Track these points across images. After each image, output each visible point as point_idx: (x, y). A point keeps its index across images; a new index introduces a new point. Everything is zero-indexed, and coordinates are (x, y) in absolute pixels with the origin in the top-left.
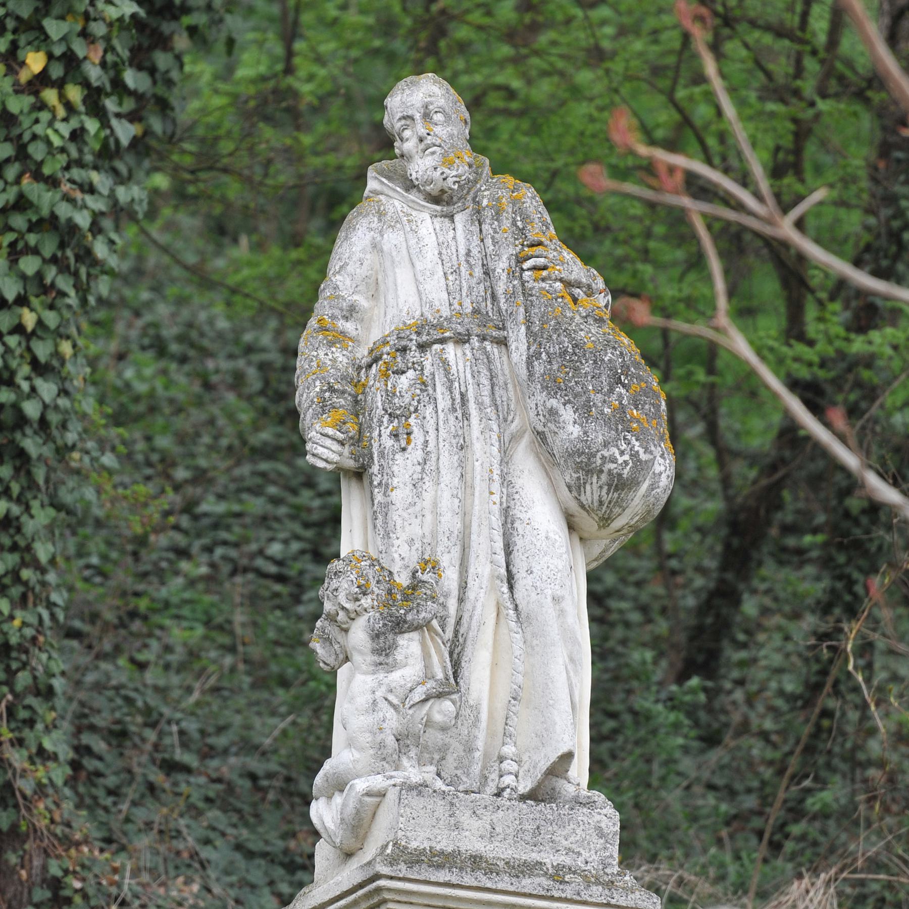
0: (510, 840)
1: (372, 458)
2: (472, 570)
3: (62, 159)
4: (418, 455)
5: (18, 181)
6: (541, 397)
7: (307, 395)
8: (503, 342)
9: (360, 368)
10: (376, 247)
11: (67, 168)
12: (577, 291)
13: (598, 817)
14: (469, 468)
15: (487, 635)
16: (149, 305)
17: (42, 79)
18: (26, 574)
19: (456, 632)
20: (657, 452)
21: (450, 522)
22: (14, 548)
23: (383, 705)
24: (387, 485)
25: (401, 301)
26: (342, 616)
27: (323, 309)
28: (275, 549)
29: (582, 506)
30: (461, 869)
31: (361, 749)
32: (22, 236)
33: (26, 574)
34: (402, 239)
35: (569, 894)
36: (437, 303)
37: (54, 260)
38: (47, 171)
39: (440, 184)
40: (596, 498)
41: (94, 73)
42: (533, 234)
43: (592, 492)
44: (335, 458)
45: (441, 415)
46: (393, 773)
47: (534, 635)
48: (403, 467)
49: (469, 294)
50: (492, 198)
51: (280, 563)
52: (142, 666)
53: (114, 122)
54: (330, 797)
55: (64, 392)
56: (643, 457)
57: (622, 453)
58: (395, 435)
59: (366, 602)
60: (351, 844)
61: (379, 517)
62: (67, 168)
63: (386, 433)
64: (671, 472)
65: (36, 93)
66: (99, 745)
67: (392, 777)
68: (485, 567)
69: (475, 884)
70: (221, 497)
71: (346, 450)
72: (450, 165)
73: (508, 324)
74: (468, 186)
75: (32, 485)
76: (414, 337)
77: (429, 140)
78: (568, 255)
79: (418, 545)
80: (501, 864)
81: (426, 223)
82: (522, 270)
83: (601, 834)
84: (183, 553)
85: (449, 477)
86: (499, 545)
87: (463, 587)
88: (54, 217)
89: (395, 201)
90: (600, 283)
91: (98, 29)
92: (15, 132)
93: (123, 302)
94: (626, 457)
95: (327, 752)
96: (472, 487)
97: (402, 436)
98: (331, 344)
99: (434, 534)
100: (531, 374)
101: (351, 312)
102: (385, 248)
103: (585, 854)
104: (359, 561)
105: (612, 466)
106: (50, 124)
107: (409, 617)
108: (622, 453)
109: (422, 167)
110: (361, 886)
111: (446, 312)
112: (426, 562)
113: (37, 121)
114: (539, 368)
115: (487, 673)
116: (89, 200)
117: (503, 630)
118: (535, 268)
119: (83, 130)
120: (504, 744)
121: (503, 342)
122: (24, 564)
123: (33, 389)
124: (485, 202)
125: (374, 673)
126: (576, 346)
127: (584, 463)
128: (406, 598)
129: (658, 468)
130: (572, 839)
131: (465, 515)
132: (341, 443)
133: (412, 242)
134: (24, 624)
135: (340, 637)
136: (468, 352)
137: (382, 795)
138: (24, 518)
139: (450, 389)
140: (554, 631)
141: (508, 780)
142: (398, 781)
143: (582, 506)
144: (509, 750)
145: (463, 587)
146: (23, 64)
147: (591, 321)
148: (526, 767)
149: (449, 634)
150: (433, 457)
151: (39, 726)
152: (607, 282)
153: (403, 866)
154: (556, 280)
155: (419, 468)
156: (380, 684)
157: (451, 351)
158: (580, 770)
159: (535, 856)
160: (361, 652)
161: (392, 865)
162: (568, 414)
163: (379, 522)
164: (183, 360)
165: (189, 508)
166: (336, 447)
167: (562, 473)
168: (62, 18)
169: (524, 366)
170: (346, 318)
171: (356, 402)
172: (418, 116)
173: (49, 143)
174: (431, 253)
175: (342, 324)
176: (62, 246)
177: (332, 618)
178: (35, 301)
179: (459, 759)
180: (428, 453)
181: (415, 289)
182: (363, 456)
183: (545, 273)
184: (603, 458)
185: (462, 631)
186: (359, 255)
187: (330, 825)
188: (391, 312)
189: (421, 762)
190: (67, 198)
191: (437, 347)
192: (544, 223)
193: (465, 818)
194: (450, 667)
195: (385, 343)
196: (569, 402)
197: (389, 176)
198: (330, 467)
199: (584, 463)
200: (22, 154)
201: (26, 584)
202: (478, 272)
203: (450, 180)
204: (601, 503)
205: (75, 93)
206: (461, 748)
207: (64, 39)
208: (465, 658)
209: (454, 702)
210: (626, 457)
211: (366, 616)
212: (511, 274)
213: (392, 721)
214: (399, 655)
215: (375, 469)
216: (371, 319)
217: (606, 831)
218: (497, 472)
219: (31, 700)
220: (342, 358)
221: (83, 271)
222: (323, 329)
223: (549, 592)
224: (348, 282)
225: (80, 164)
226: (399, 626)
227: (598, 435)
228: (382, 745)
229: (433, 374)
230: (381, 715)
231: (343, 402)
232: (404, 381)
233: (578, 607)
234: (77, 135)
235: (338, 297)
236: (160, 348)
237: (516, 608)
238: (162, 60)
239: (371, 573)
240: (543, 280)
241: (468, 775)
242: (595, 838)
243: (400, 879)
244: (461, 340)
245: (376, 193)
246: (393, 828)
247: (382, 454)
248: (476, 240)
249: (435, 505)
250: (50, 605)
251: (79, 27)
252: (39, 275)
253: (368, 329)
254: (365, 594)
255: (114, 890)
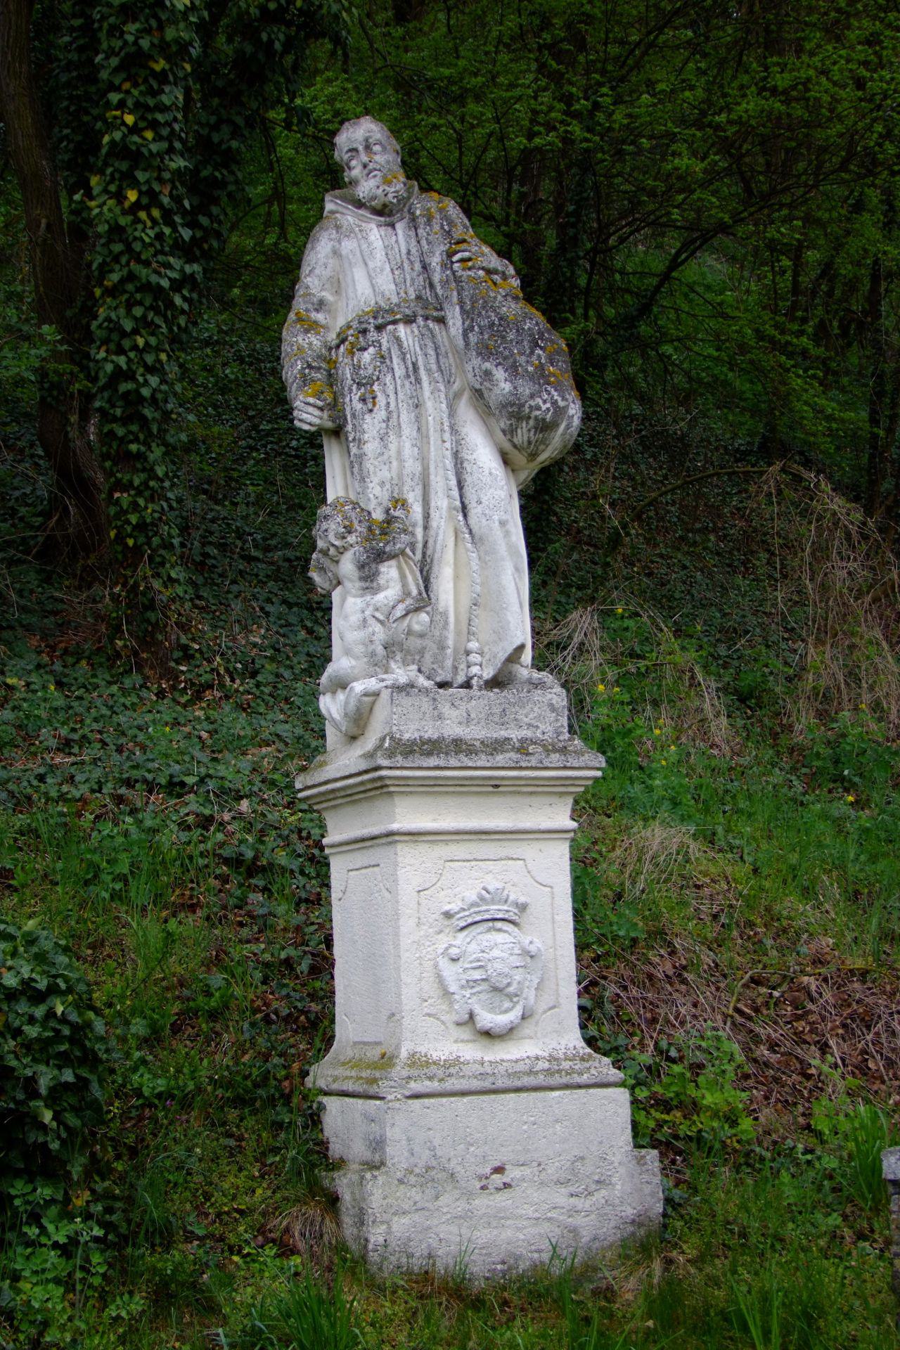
0: (483, 723)
1: (346, 419)
2: (433, 504)
3: (152, 250)
4: (383, 414)
5: (128, 264)
6: (476, 361)
7: (292, 370)
8: (441, 321)
9: (330, 349)
10: (336, 253)
11: (155, 255)
12: (495, 277)
13: (550, 696)
14: (423, 422)
15: (449, 556)
16: (236, 343)
17: (137, 206)
18: (152, 483)
19: (424, 554)
20: (570, 399)
21: (412, 466)
22: (144, 470)
23: (371, 621)
24: (360, 440)
25: (359, 293)
26: (332, 551)
27: (299, 304)
28: (294, 443)
29: (515, 446)
30: (447, 754)
31: (357, 658)
32: (132, 294)
33: (152, 483)
34: (355, 245)
35: (533, 764)
36: (387, 293)
37: (151, 308)
38: (143, 257)
39: (383, 199)
40: (526, 439)
41: (166, 200)
42: (458, 233)
43: (522, 435)
44: (317, 421)
45: (399, 382)
46: (385, 676)
47: (487, 553)
48: (372, 425)
49: (413, 284)
50: (423, 209)
51: (296, 450)
52: (236, 504)
53: (180, 229)
54: (334, 693)
55: (163, 381)
56: (561, 404)
57: (545, 402)
58: (363, 400)
59: (351, 539)
60: (355, 731)
61: (355, 465)
62: (155, 255)
63: (356, 398)
64: (579, 414)
65: (135, 214)
66: (214, 551)
67: (383, 680)
68: (442, 502)
69: (459, 765)
70: (268, 422)
71: (325, 415)
72: (389, 183)
73: (445, 306)
74: (403, 201)
75: (150, 434)
76: (372, 321)
77: (371, 166)
78: (486, 250)
79: (388, 486)
80: (477, 744)
81: (375, 233)
82: (452, 263)
83: (553, 708)
84: (252, 448)
85: (408, 430)
86: (454, 482)
87: (427, 516)
88: (149, 283)
89: (349, 217)
90: (511, 270)
91: (167, 175)
92: (124, 237)
93: (225, 343)
94: (548, 405)
95: (329, 660)
96: (428, 437)
97: (369, 400)
98: (307, 331)
99: (400, 476)
100: (467, 344)
101: (321, 305)
102: (344, 253)
103: (542, 727)
104: (343, 506)
105: (538, 413)
106: (143, 230)
107: (387, 549)
108: (545, 402)
109: (367, 187)
110: (366, 772)
111: (395, 300)
112: (397, 501)
113: (136, 229)
114: (473, 338)
115: (451, 585)
116: (169, 273)
117: (461, 550)
118: (462, 260)
119: (163, 233)
120: (469, 641)
121: (441, 321)
122: (150, 478)
123: (146, 381)
124: (418, 212)
125: (362, 596)
126: (501, 319)
127: (515, 412)
128: (384, 533)
129: (571, 412)
130: (531, 716)
131: (424, 459)
132: (321, 409)
133: (364, 246)
134: (154, 511)
135: (332, 567)
136: (415, 330)
137: (377, 694)
138: (148, 453)
139: (404, 360)
140: (502, 549)
141: (475, 670)
142: (389, 683)
143: (515, 446)
144: (473, 645)
145: (427, 516)
146: (126, 198)
147: (509, 299)
148: (487, 657)
149: (419, 556)
150: (395, 415)
151: (168, 565)
152: (516, 269)
153: (399, 758)
154: (479, 268)
155: (384, 425)
156: (368, 605)
157: (402, 330)
158: (527, 657)
159: (504, 734)
160: (350, 580)
161: (390, 757)
162: (500, 374)
163: (356, 470)
164: (251, 364)
165: (255, 427)
166: (317, 412)
167: (498, 421)
168: (145, 170)
169: (461, 337)
170: (317, 311)
171: (330, 375)
172: (361, 148)
173: (143, 241)
174: (380, 255)
175: (314, 315)
176: (155, 299)
177: (325, 553)
178: (143, 332)
179: (435, 656)
180: (390, 413)
181: (369, 284)
182: (339, 418)
183: (470, 264)
184: (531, 407)
185: (429, 552)
186: (323, 260)
187: (336, 716)
188: (352, 303)
189: (405, 663)
190: (159, 273)
191: (390, 327)
192: (465, 226)
193: (446, 710)
194: (421, 582)
195: (349, 327)
196: (499, 364)
197: (344, 199)
198: (313, 429)
199: (515, 412)
200: (129, 249)
201: (152, 489)
202: (418, 266)
203: (390, 196)
204: (529, 443)
205: (156, 213)
206: (435, 646)
207: (148, 182)
208: (433, 575)
209: (428, 613)
210: (548, 405)
211: (352, 551)
212: (444, 266)
213: (380, 633)
214: (382, 580)
215: (349, 427)
216: (336, 310)
217: (557, 706)
218: (446, 424)
219: (162, 552)
220: (315, 341)
221: (169, 313)
222: (300, 319)
223: (496, 517)
224: (316, 282)
225: (162, 252)
226: (380, 556)
227: (526, 389)
228: (373, 654)
229: (389, 349)
230: (370, 629)
231: (319, 376)
232: (367, 356)
233: (516, 526)
234: (160, 236)
235: (310, 294)
236: (241, 360)
237: (471, 532)
238: (215, 210)
239: (353, 515)
240: (470, 269)
241: (443, 668)
242: (548, 713)
243: (398, 768)
244: (409, 320)
245: (333, 212)
246: (388, 723)
247: (354, 416)
248: (413, 242)
249: (399, 452)
250: (167, 500)
251: (155, 175)
252: (144, 317)
253: (335, 318)
254: (350, 532)
255: (217, 648)
